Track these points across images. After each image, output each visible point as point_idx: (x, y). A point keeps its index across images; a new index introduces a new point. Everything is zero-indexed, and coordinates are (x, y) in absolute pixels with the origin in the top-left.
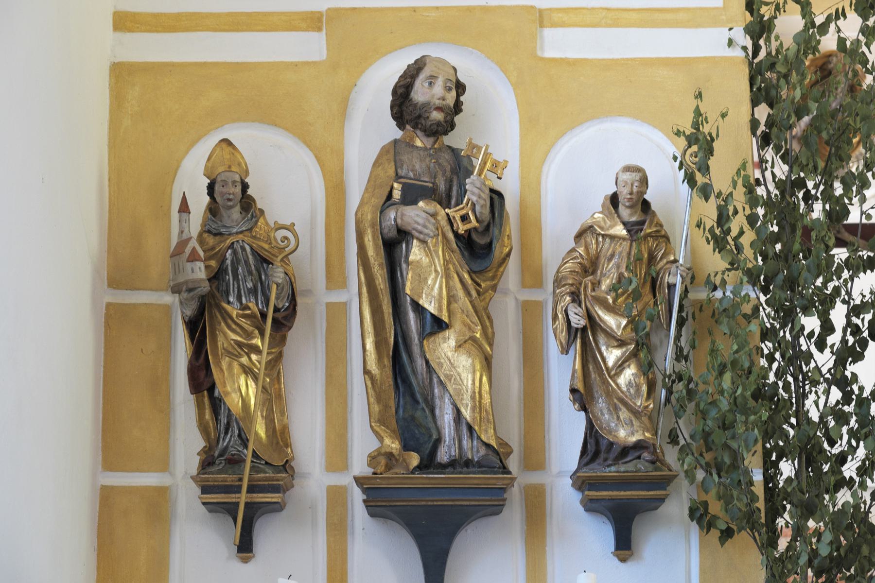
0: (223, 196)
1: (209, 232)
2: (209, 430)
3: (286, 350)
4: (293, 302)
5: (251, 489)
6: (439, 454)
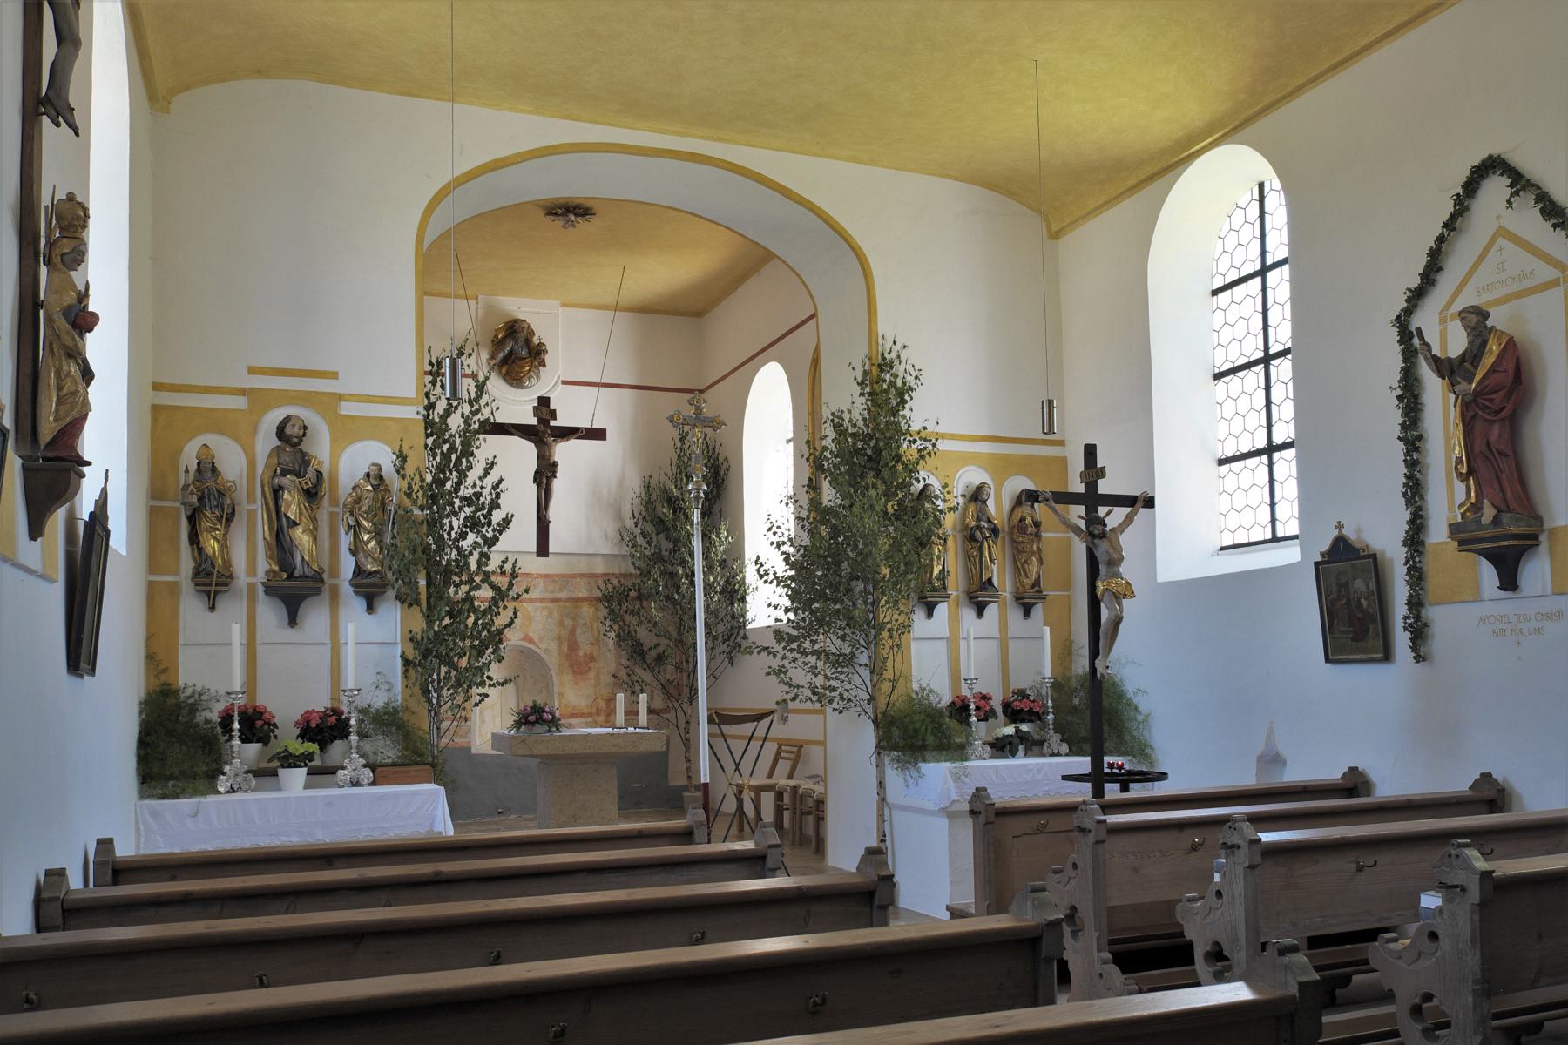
5: (217, 585)
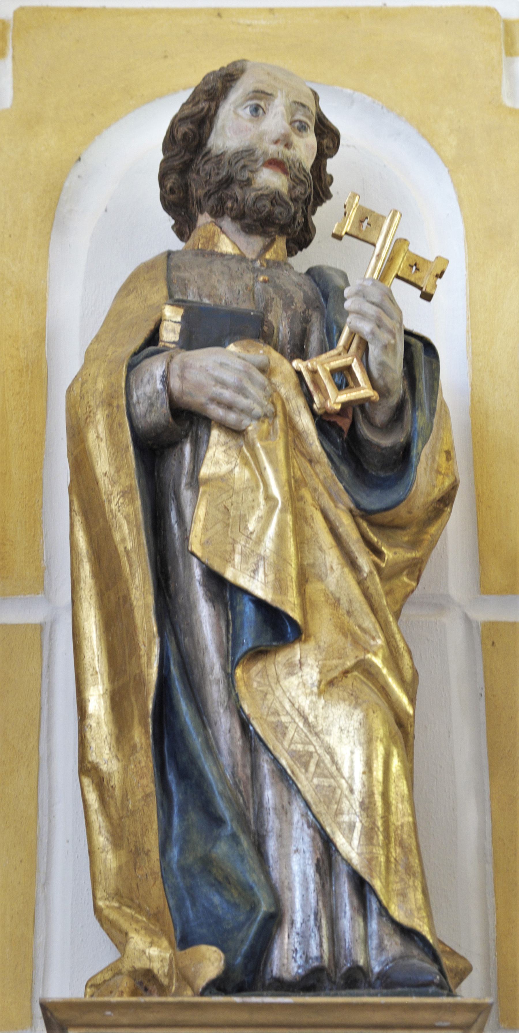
6: (276, 953)
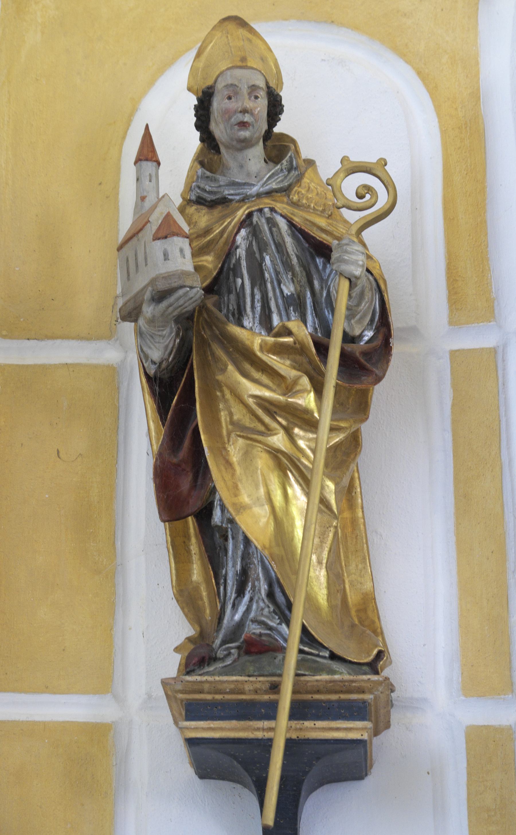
0: (230, 118)
1: (200, 201)
2: (200, 602)
3: (365, 428)
4: (383, 330)
